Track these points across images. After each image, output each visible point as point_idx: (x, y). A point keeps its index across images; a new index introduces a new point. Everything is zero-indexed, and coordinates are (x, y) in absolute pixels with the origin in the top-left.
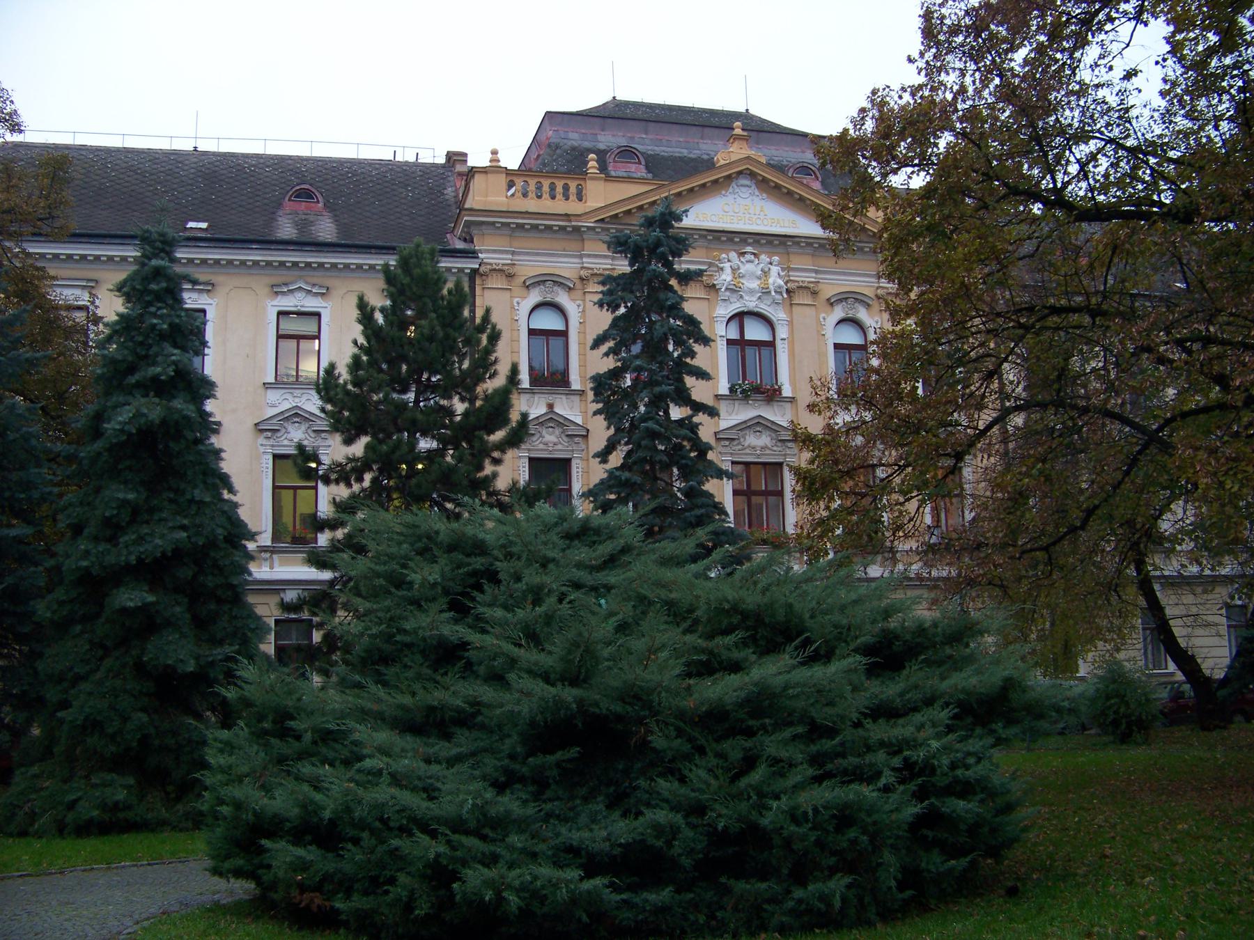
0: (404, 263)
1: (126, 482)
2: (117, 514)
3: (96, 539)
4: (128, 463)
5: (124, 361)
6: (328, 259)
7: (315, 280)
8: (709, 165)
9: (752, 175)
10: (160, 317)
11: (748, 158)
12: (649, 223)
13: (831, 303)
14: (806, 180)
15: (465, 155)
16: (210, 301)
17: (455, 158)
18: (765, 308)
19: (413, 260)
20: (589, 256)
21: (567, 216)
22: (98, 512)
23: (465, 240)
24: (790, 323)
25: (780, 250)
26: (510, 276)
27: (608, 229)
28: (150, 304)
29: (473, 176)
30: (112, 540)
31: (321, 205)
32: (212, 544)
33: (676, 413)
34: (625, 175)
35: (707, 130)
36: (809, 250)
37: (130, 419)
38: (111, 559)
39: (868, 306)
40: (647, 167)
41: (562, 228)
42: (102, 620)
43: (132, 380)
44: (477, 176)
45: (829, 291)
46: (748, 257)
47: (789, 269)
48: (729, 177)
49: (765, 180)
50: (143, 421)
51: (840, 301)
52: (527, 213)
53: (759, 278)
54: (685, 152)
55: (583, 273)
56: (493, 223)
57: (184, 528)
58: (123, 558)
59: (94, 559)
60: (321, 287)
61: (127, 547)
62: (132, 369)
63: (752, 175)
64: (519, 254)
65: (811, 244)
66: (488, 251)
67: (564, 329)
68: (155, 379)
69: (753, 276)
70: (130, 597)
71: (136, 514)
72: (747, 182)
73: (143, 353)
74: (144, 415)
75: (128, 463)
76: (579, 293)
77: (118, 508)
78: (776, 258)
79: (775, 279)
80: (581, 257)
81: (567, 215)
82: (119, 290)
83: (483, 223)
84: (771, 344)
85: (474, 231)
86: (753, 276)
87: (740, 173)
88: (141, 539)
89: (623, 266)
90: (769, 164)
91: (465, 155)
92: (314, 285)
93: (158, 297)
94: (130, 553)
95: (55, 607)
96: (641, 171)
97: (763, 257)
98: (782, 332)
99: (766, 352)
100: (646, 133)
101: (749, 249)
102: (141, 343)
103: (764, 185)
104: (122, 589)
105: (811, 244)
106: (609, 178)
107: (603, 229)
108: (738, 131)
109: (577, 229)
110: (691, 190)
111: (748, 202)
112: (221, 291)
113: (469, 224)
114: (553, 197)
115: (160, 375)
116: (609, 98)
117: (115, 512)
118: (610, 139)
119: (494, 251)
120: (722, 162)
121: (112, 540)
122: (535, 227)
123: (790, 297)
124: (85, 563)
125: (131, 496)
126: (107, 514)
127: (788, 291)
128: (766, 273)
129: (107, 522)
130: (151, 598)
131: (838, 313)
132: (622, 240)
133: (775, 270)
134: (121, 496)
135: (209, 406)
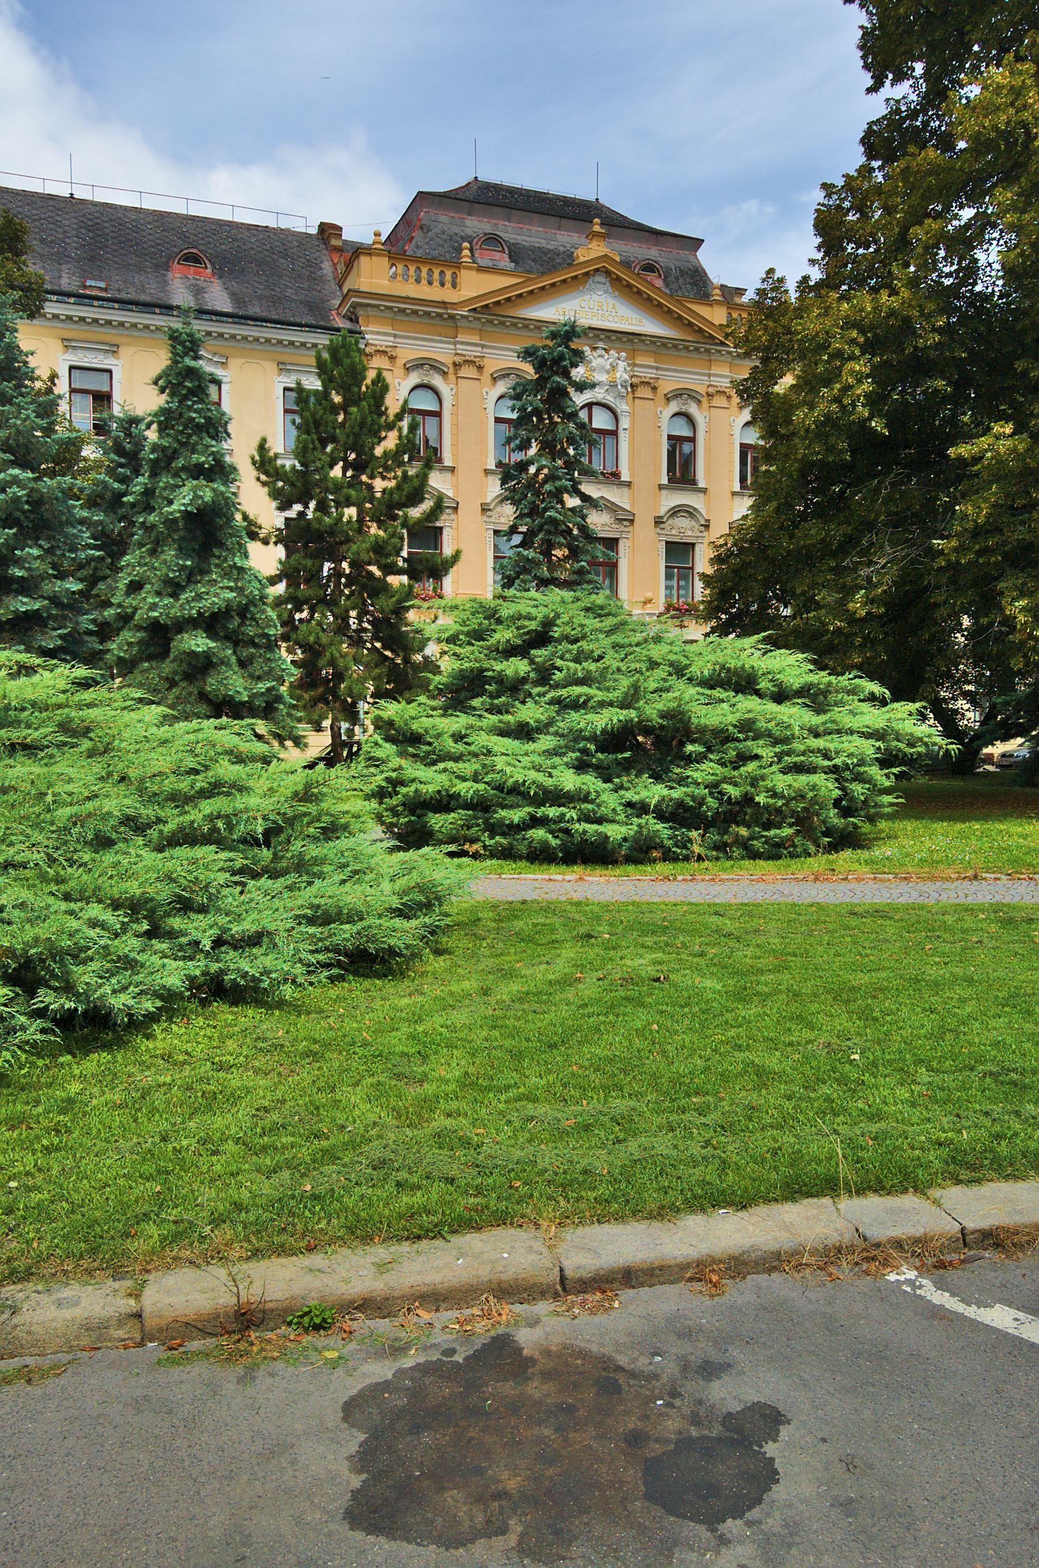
0: (333, 350)
6: (228, 329)
7: (219, 350)
8: (568, 259)
9: (608, 273)
10: (195, 411)
11: (606, 256)
12: (553, 336)
13: (668, 399)
14: (651, 277)
15: (341, 229)
16: (115, 362)
17: (328, 231)
18: (610, 399)
19: (342, 351)
20: (462, 343)
21: (444, 304)
23: (351, 320)
24: (632, 415)
25: (629, 347)
26: (392, 358)
27: (479, 319)
28: (186, 398)
29: (358, 257)
30: (175, 595)
31: (209, 271)
32: (252, 602)
33: (572, 502)
34: (490, 264)
35: (564, 221)
36: (652, 348)
39: (699, 402)
40: (510, 257)
41: (439, 315)
44: (364, 260)
45: (666, 386)
46: (600, 352)
47: (635, 365)
48: (587, 274)
49: (618, 279)
51: (676, 396)
52: (408, 298)
53: (608, 372)
54: (544, 243)
55: (457, 359)
56: (378, 306)
57: (231, 589)
60: (222, 356)
63: (608, 273)
64: (400, 337)
65: (654, 343)
66: (373, 333)
68: (199, 466)
69: (602, 369)
70: (198, 642)
71: (192, 576)
72: (603, 280)
76: (452, 377)
77: (179, 571)
78: (624, 354)
79: (622, 374)
80: (455, 344)
81: (444, 303)
82: (156, 383)
83: (368, 305)
84: (614, 433)
85: (360, 312)
86: (602, 369)
87: (597, 270)
88: (199, 597)
89: (529, 370)
90: (621, 262)
92: (215, 354)
93: (192, 392)
94: (192, 608)
96: (505, 262)
97: (612, 352)
98: (625, 423)
99: (609, 440)
100: (509, 221)
101: (601, 344)
102: (182, 432)
103: (617, 283)
105: (654, 343)
106: (481, 269)
107: (475, 318)
108: (597, 228)
109: (452, 317)
110: (553, 285)
111: (602, 299)
112: (125, 352)
113: (355, 306)
114: (430, 283)
115: (203, 463)
116: (470, 178)
118: (477, 225)
119: (378, 333)
120: (582, 259)
121: (175, 595)
122: (415, 312)
123: (633, 391)
125: (189, 563)
127: (632, 386)
128: (614, 368)
129: (167, 582)
130: (212, 644)
131: (674, 407)
132: (531, 351)
133: (622, 365)
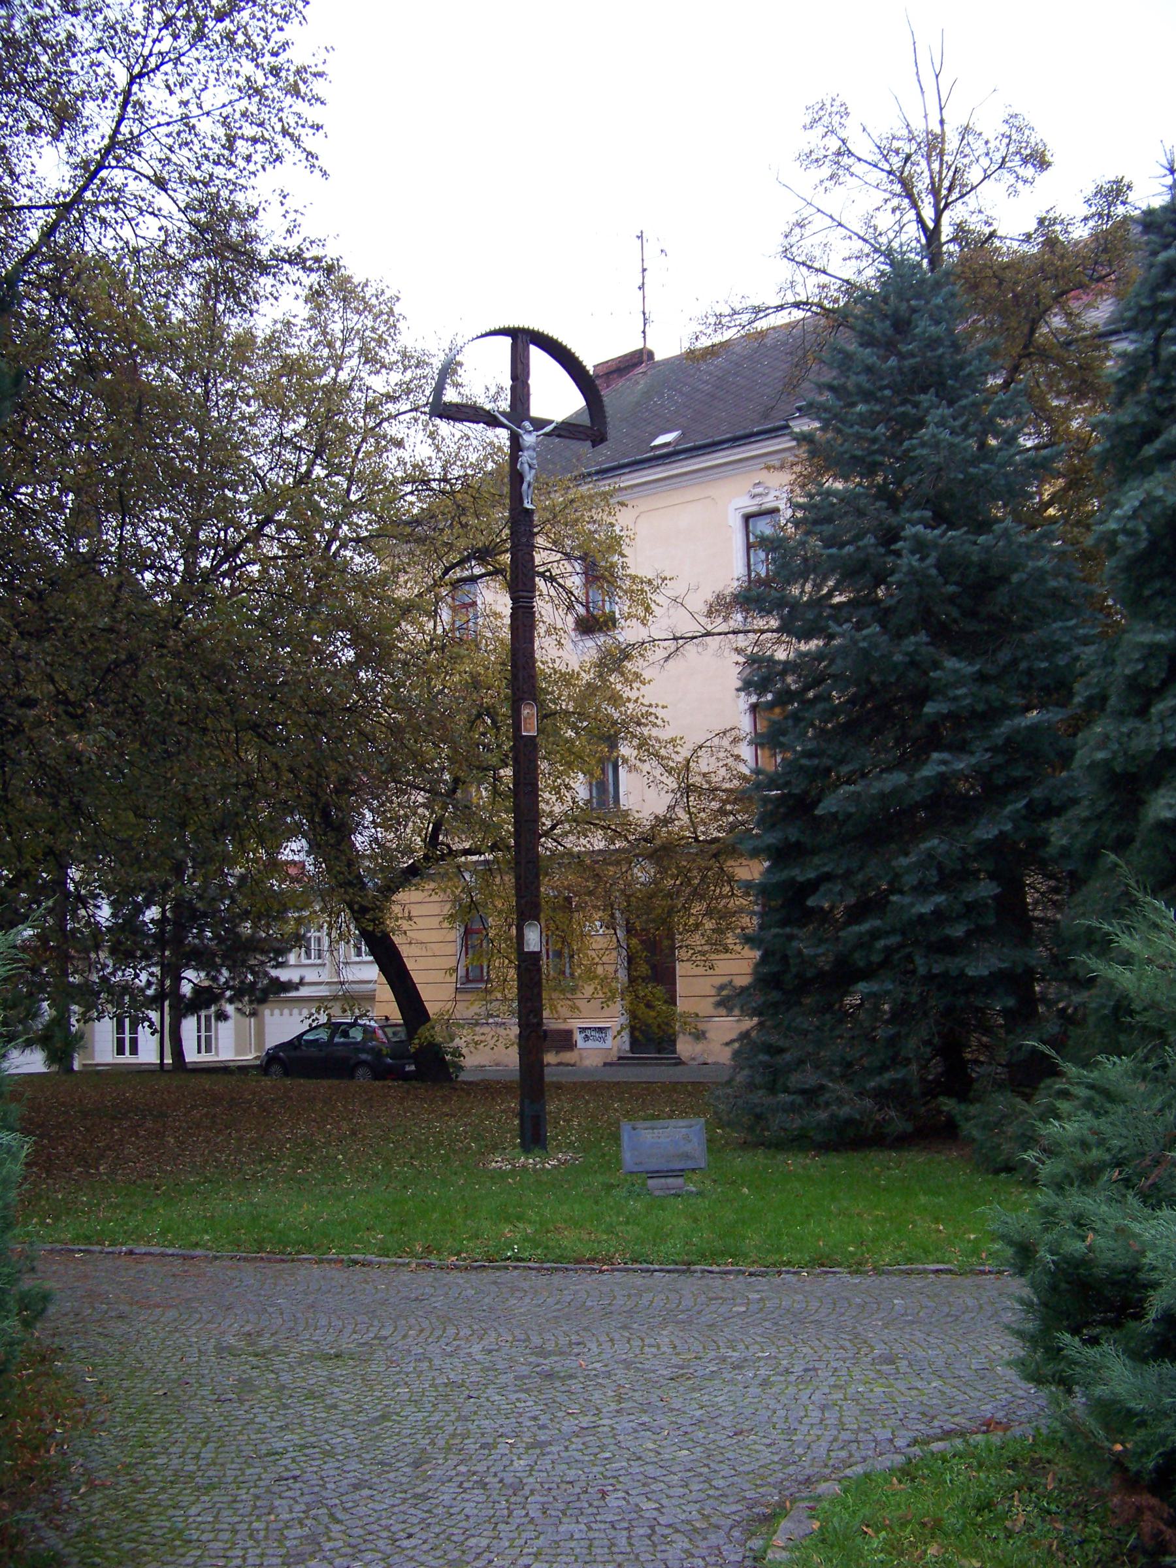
1: (1156, 618)
2: (1145, 669)
3: (1121, 715)
4: (1157, 585)
5: (1134, 424)
22: (1117, 671)
30: (1142, 712)
37: (1135, 511)
38: (1138, 744)
42: (1137, 844)
43: (1149, 450)
50: (1157, 509)
58: (1157, 740)
59: (1116, 747)
61: (1161, 721)
62: (1150, 434)
67: (507, 341)
73: (1166, 405)
74: (1159, 500)
75: (1157, 585)
77: (1143, 659)
91: (1049, 165)
95: (1076, 828)
104: (1162, 791)
117: (1140, 667)
124: (1100, 755)
125: (1160, 638)
126: (1127, 671)
134: (1145, 638)
135: (658, 357)
